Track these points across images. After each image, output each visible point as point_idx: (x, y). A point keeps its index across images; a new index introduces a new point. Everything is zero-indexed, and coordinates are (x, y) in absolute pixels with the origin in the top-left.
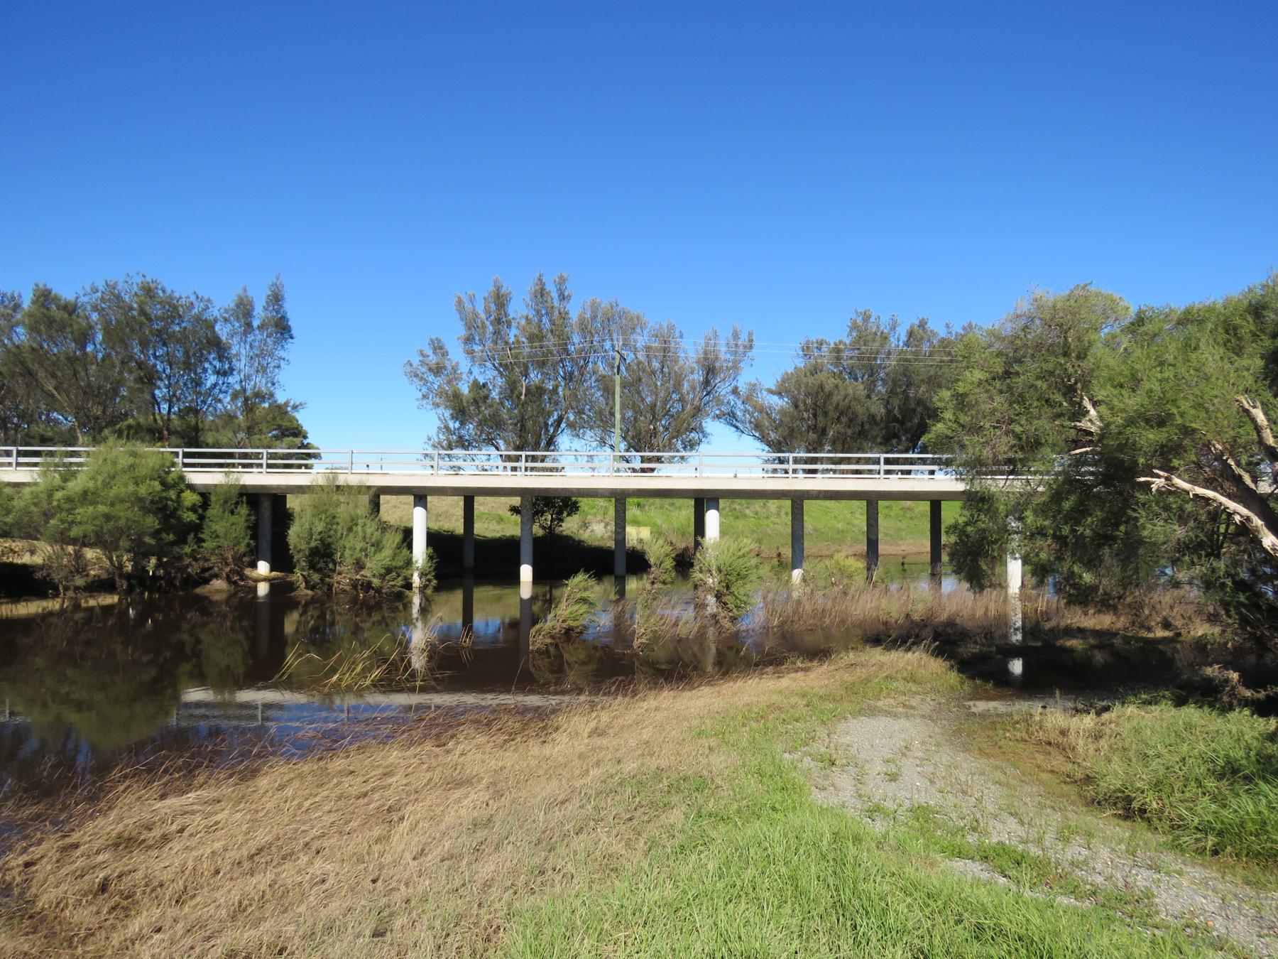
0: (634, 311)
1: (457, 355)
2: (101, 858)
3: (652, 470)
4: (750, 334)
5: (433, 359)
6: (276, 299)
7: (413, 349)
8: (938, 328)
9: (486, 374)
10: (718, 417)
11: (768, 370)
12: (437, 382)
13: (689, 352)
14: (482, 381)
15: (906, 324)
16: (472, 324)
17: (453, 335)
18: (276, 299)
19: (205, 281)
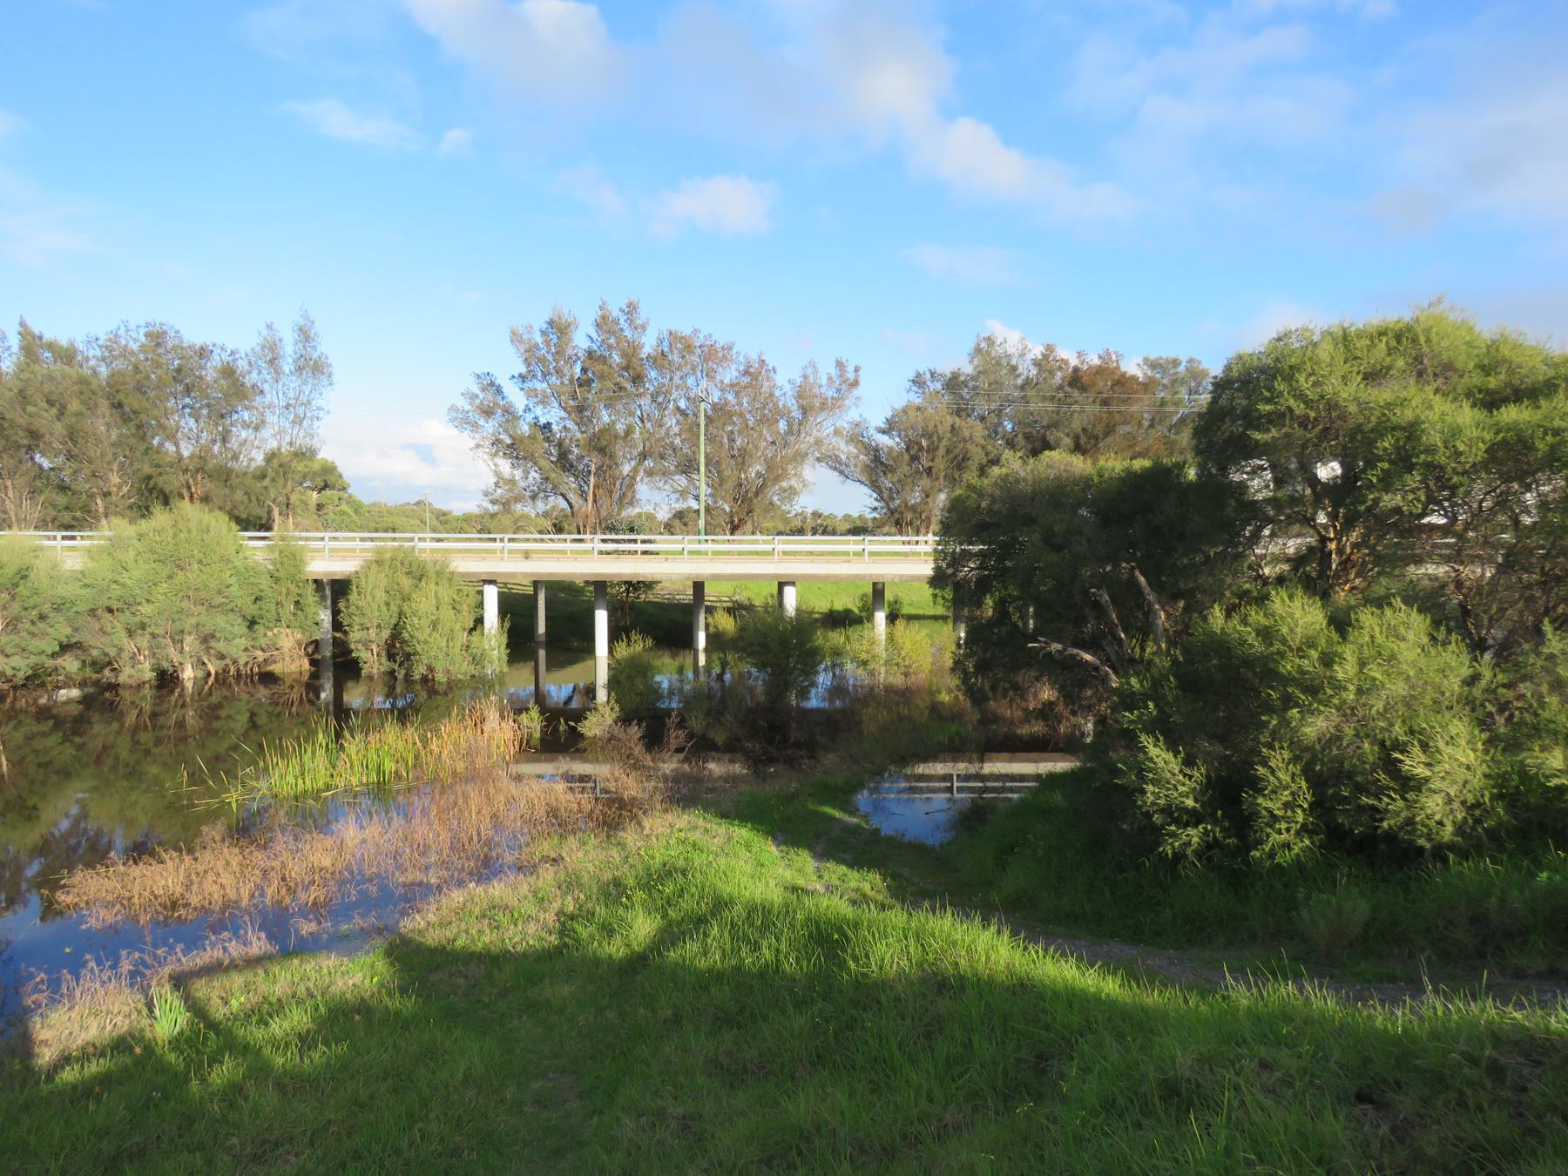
0: (721, 339)
1: (516, 397)
2: (372, 755)
3: (323, 598)
4: (857, 369)
5: (486, 398)
6: (305, 335)
7: (459, 387)
8: (1068, 356)
9: (553, 415)
10: (819, 460)
11: (878, 403)
12: (490, 426)
13: (784, 381)
14: (543, 421)
15: (1037, 351)
16: (531, 355)
17: (507, 366)
18: (305, 335)
19: (219, 320)
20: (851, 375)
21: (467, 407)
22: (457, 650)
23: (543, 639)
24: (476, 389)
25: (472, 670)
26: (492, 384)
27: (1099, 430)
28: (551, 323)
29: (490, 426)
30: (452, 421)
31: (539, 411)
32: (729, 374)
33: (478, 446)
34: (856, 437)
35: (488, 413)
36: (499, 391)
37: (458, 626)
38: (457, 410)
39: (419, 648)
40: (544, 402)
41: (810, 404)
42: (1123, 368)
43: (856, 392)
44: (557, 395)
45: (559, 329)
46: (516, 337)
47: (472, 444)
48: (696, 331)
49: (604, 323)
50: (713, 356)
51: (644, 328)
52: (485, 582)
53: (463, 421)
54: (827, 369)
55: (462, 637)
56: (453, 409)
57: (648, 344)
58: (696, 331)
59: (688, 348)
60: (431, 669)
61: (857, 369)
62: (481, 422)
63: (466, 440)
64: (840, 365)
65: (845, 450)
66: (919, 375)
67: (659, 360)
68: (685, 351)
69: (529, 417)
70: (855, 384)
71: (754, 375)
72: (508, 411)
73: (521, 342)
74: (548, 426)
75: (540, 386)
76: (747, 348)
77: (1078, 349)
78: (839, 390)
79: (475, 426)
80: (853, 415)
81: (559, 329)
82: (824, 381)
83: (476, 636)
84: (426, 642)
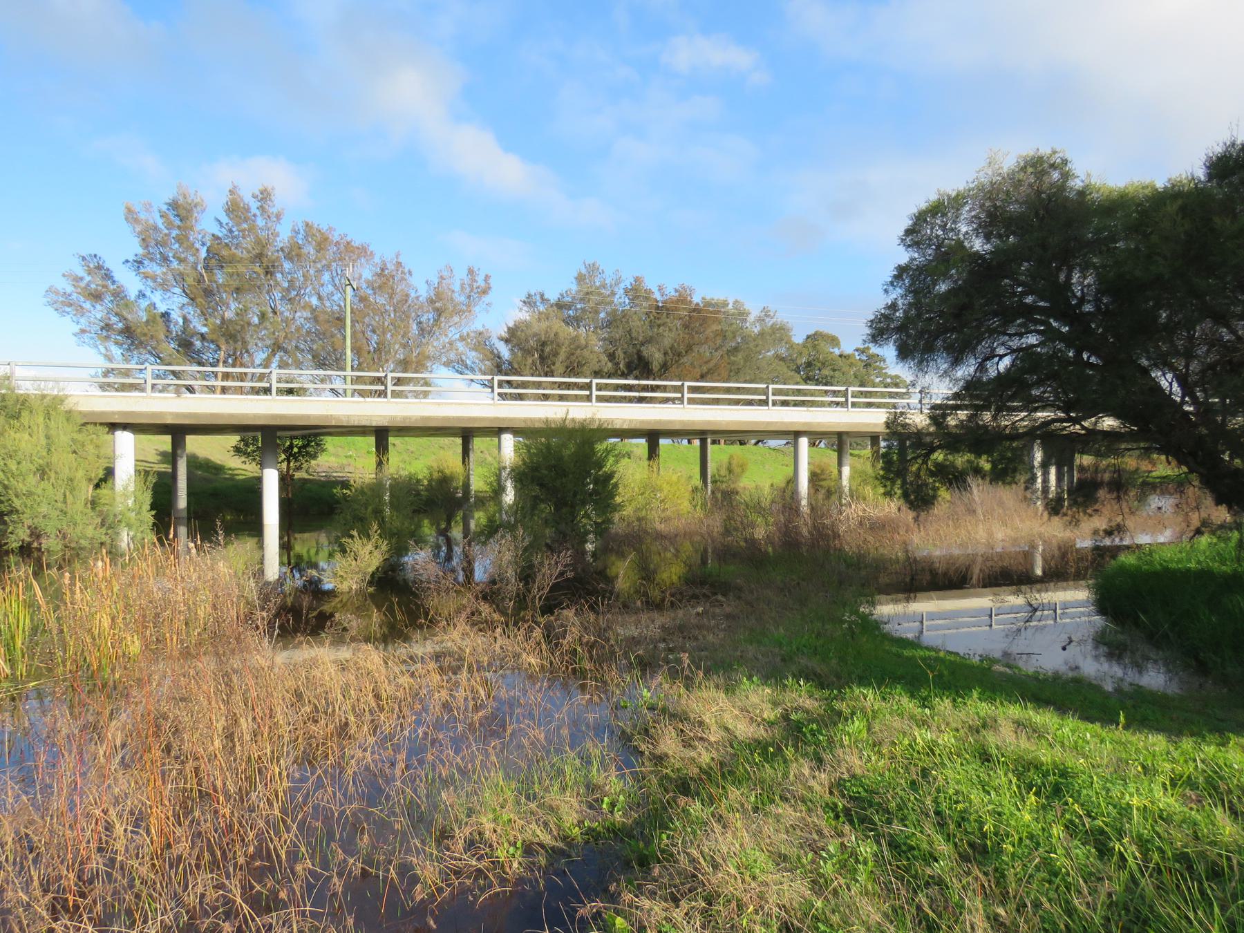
1: (131, 283)
4: (487, 278)
5: (96, 283)
7: (60, 266)
12: (98, 312)
13: (419, 286)
14: (162, 308)
16: (147, 237)
17: (117, 252)
20: (481, 282)
21: (69, 289)
22: (80, 506)
23: (185, 514)
24: (81, 272)
25: (101, 534)
26: (100, 267)
27: (682, 349)
28: (174, 205)
29: (98, 312)
30: (49, 304)
31: (157, 297)
32: (366, 272)
33: (83, 331)
34: (480, 342)
35: (96, 297)
36: (108, 276)
37: (80, 474)
38: (57, 293)
39: (17, 503)
40: (164, 287)
41: (441, 307)
42: (367, 481)
43: (486, 299)
44: (180, 277)
45: (181, 211)
46: (131, 216)
47: (76, 328)
48: (330, 229)
49: (235, 209)
50: (352, 252)
51: (278, 216)
52: (113, 427)
53: (63, 304)
54: (461, 274)
55: (88, 491)
56: (51, 290)
57: (284, 234)
58: (330, 229)
59: (322, 243)
60: (36, 534)
61: (487, 278)
62: (87, 305)
63: (68, 325)
64: (471, 272)
65: (472, 357)
66: (529, 296)
67: (293, 253)
68: (318, 245)
69: (144, 304)
70: (485, 292)
71: (386, 280)
72: (119, 295)
73: (136, 221)
74: (166, 315)
75: (157, 270)
76: (384, 250)
77: (663, 282)
78: (469, 297)
79: (80, 311)
80: (477, 325)
81: (181, 211)
82: (457, 288)
83: (104, 491)
84: (30, 494)
